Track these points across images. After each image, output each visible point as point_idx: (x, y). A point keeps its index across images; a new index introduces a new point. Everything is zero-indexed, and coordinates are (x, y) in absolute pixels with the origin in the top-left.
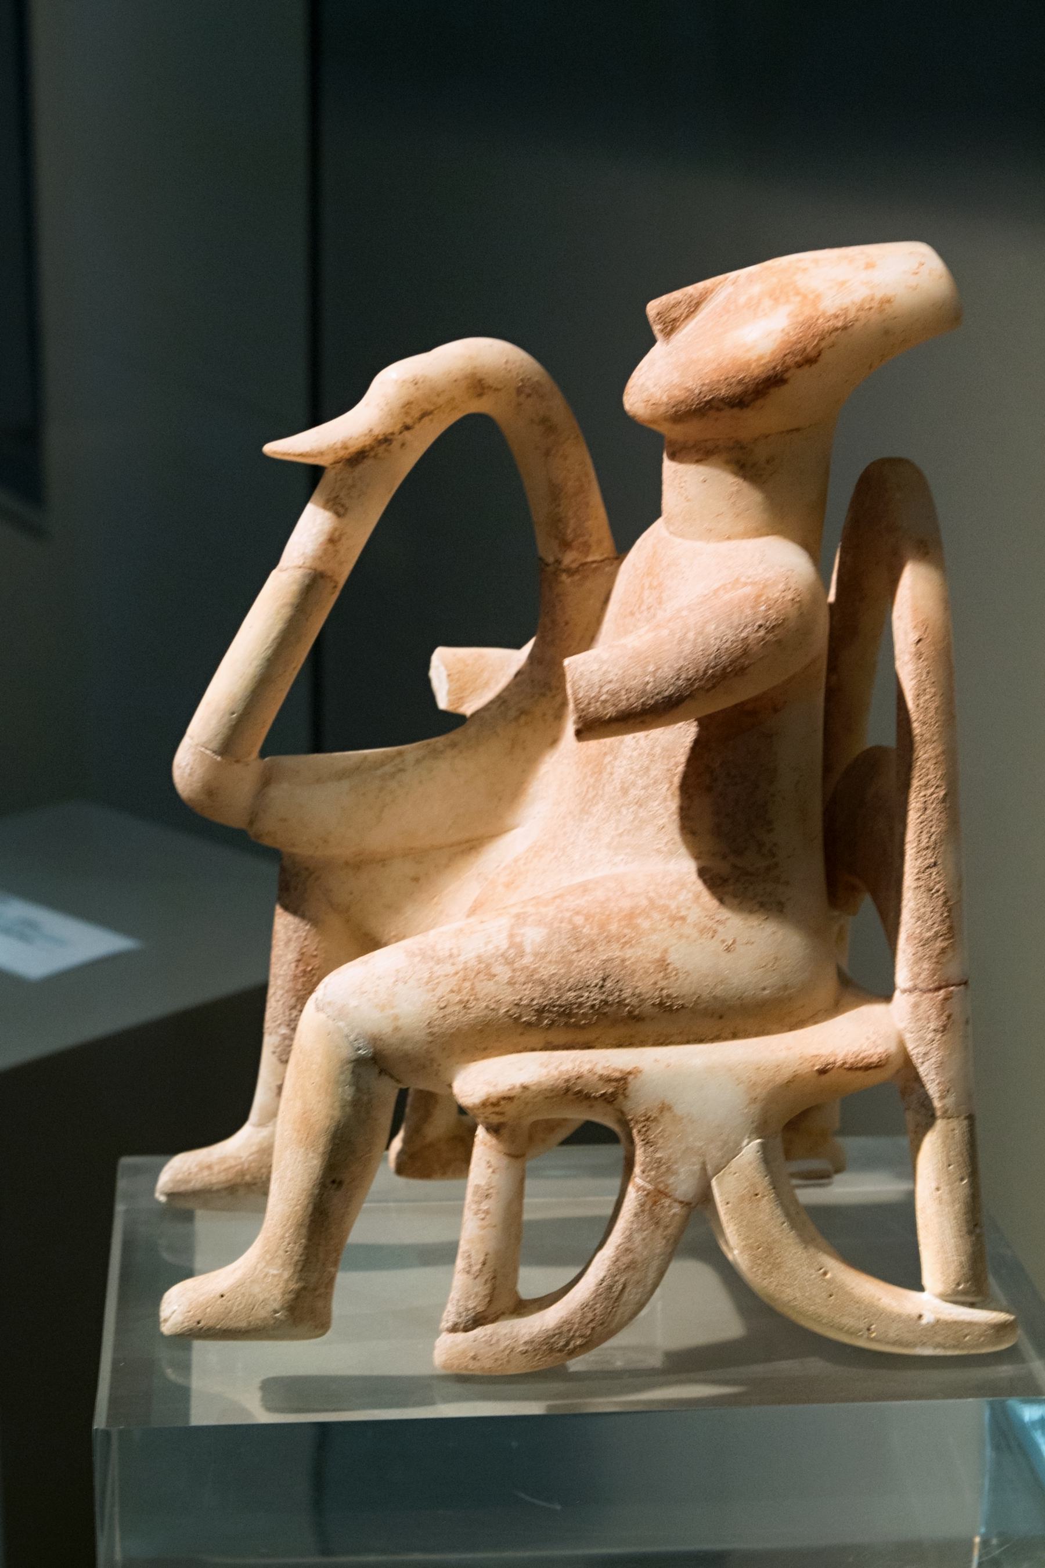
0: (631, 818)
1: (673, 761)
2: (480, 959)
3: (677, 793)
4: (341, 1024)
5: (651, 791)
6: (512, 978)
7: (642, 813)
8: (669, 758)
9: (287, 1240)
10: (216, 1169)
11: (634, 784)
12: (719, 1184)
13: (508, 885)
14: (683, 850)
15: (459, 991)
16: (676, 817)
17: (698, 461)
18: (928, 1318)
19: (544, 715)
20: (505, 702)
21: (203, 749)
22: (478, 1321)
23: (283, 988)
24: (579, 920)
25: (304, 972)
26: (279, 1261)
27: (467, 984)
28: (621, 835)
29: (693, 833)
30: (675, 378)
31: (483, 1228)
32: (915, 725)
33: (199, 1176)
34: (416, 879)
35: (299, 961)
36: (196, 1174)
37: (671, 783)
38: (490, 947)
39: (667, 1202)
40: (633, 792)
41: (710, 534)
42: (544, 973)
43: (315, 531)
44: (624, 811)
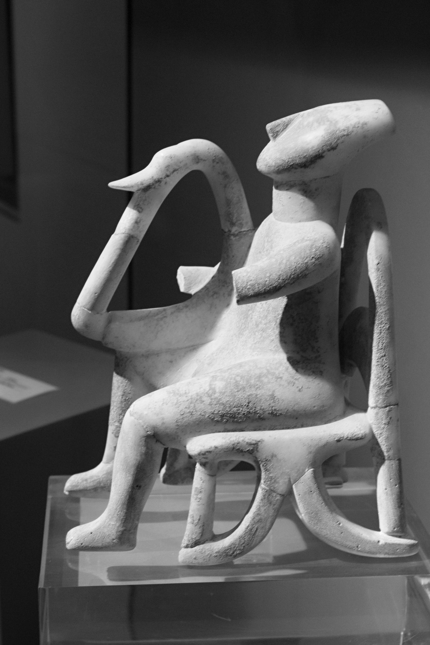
0: (260, 336)
1: (277, 313)
2: (197, 394)
3: (279, 326)
4: (140, 421)
5: (268, 325)
6: (211, 402)
7: (264, 334)
8: (275, 312)
9: (118, 510)
10: (89, 481)
11: (261, 322)
12: (296, 487)
13: (209, 364)
14: (281, 350)
15: (189, 408)
16: (278, 336)
17: (287, 190)
18: (382, 542)
19: (224, 294)
20: (208, 289)
21: (83, 308)
22: (196, 543)
23: (116, 406)
24: (238, 379)
25: (125, 400)
26: (115, 519)
27: (192, 405)
28: (255, 343)
29: (285, 343)
30: (278, 155)
31: (199, 505)
32: (376, 298)
33: (82, 484)
34: (171, 362)
35: (123, 395)
36: (81, 483)
37: (276, 322)
38: (202, 389)
39: (274, 494)
40: (261, 326)
41: (292, 220)
42: (224, 400)
43: (129, 218)
44: (257, 334)
